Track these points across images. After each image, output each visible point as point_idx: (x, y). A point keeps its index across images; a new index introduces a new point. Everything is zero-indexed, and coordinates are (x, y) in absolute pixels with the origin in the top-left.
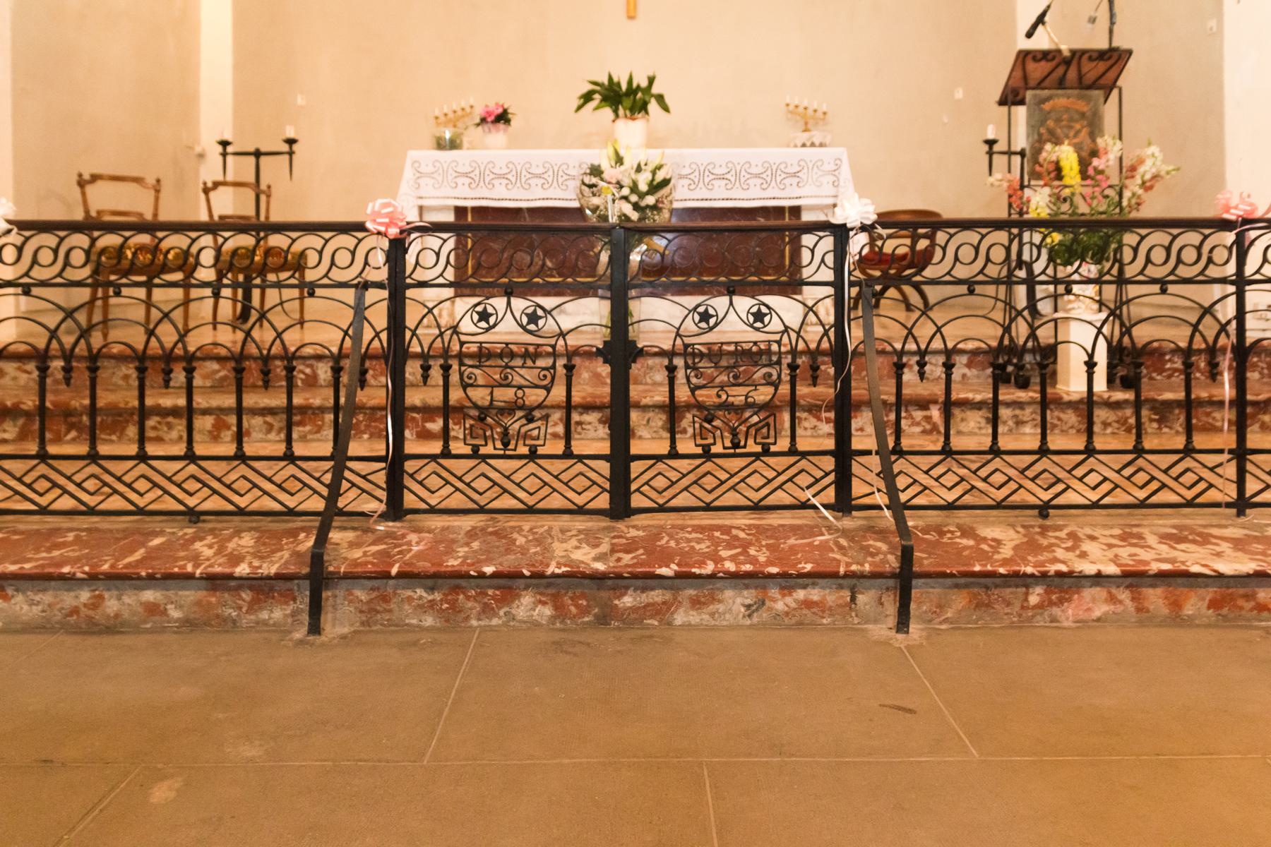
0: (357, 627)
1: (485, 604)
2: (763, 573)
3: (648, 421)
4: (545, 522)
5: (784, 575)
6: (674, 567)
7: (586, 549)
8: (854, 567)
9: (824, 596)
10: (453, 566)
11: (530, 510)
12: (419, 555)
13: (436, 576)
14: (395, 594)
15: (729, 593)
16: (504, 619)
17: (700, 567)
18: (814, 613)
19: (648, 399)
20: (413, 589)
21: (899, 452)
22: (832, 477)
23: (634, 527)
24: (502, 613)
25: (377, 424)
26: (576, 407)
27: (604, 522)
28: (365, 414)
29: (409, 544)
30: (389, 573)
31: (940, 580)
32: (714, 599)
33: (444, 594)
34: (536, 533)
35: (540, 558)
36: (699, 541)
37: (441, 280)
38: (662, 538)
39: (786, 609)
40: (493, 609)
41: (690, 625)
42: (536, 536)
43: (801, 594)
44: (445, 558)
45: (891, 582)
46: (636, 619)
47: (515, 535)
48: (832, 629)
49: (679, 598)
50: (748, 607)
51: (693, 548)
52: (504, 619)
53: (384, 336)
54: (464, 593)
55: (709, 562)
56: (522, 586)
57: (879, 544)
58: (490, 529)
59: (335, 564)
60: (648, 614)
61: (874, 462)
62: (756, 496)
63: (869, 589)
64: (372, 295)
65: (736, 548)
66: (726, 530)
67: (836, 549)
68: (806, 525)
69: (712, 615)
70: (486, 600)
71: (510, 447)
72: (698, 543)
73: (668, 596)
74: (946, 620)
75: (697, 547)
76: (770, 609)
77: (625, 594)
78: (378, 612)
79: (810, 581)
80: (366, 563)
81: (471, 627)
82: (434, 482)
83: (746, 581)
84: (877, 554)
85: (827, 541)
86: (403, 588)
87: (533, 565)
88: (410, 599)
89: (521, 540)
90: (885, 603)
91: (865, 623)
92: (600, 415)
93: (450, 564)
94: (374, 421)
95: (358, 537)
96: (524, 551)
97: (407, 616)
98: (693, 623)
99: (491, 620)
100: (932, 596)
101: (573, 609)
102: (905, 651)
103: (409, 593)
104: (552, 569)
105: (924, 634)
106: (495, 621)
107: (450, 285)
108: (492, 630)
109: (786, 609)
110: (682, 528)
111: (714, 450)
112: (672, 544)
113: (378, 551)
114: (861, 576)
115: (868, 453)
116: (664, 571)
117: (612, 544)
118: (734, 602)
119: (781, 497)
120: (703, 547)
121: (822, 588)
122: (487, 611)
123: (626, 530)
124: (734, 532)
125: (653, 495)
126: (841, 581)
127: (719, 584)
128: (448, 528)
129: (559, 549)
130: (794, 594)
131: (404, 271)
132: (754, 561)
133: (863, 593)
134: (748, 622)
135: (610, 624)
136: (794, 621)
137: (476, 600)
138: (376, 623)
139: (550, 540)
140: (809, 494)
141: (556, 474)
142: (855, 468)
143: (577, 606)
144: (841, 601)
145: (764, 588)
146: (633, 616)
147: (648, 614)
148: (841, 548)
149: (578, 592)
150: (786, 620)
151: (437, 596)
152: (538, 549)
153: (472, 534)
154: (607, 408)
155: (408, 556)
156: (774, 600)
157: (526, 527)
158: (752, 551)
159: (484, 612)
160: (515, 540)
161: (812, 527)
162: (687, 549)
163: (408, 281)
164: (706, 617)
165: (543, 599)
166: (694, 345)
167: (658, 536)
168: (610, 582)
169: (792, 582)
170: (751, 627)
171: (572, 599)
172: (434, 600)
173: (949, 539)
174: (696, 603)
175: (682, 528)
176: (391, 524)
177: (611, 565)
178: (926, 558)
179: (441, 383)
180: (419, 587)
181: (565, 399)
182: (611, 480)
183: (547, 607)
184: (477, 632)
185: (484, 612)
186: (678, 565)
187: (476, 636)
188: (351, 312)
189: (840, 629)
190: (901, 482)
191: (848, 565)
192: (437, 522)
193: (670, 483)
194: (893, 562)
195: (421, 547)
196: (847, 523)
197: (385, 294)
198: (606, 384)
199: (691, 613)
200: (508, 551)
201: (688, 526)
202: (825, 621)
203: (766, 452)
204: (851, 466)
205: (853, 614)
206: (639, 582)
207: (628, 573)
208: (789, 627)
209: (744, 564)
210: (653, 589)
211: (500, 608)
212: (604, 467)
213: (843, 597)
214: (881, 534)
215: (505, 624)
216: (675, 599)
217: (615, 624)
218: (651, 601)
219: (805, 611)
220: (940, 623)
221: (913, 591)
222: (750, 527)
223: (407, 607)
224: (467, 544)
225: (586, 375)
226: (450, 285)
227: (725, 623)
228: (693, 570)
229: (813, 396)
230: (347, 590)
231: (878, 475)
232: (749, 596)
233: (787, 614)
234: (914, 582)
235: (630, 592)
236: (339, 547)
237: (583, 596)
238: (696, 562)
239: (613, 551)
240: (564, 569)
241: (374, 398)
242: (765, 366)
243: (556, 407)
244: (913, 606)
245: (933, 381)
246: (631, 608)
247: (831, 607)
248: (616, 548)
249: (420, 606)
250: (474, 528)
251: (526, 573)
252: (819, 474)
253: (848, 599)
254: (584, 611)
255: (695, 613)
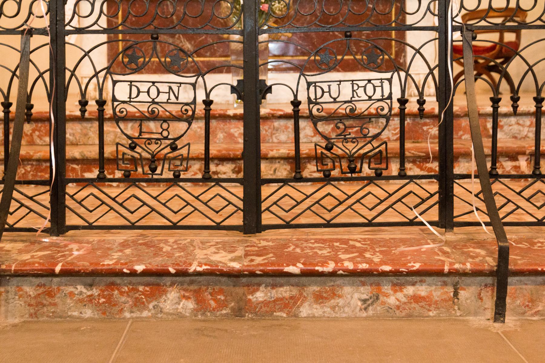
0: (27, 318)
1: (136, 298)
2: (377, 271)
3: (275, 171)
4: (187, 237)
5: (396, 273)
6: (300, 266)
7: (224, 253)
8: (457, 266)
9: (431, 291)
10: (109, 265)
11: (175, 226)
12: (79, 258)
13: (94, 274)
14: (59, 290)
15: (347, 289)
16: (153, 312)
17: (322, 266)
18: (422, 307)
19: (275, 152)
20: (75, 286)
21: (496, 177)
22: (436, 198)
23: (264, 240)
24: (151, 306)
25: (43, 174)
26: (213, 159)
27: (238, 236)
28: (32, 165)
29: (71, 250)
30: (54, 270)
31: (533, 278)
32: (335, 294)
33: (101, 290)
34: (180, 244)
35: (184, 259)
36: (321, 249)
37: (95, 28)
38: (289, 247)
39: (398, 303)
40: (143, 303)
41: (314, 317)
42: (181, 246)
43: (410, 290)
44: (102, 260)
45: (489, 280)
46: (267, 312)
47: (162, 245)
48: (437, 319)
49: (305, 294)
50: (365, 301)
51: (316, 253)
52: (153, 312)
53: (47, 76)
54: (118, 289)
55: (330, 262)
56: (168, 283)
57: (478, 250)
58: (140, 242)
59: (7, 263)
60: (277, 307)
61: (475, 185)
62: (370, 215)
63: (469, 285)
64: (36, 40)
65: (353, 253)
66: (345, 242)
67: (440, 254)
68: (414, 239)
69: (333, 308)
70: (137, 295)
71: (156, 173)
72: (320, 250)
73: (295, 291)
74: (537, 313)
75: (320, 252)
76: (383, 303)
77: (258, 290)
78: (44, 305)
79: (418, 279)
80: (34, 263)
81: (124, 318)
82: (90, 203)
83: (363, 279)
84: (477, 257)
85: (432, 249)
86: (66, 285)
87: (178, 264)
88: (71, 294)
89: (166, 248)
90: (484, 298)
91: (466, 316)
92: (234, 166)
93: (106, 263)
94: (40, 172)
95: (26, 246)
96: (169, 255)
97: (70, 308)
98: (316, 315)
99: (142, 312)
100: (525, 292)
101: (212, 303)
102: (502, 335)
103: (71, 289)
104: (194, 267)
105: (518, 323)
106: (145, 314)
107: (104, 31)
108: (143, 321)
109: (398, 303)
110: (307, 241)
111: (335, 173)
112: (298, 250)
113: (44, 255)
114: (464, 274)
115: (468, 176)
116: (291, 269)
117: (245, 251)
118: (352, 297)
119: (391, 217)
120: (325, 252)
121: (429, 285)
122: (138, 304)
123: (257, 242)
124: (351, 243)
125: (282, 213)
126: (445, 279)
127: (339, 281)
128: (104, 240)
129: (200, 254)
130: (405, 290)
131: (64, 20)
132: (369, 261)
133: (464, 290)
134: (364, 314)
135: (244, 316)
136: (404, 314)
137: (128, 296)
138: (42, 315)
139: (192, 248)
140: (416, 212)
141: (196, 195)
142: (457, 190)
143: (215, 300)
144: (444, 297)
145: (378, 285)
146: (264, 309)
147: (277, 307)
148: (445, 253)
149: (217, 288)
150: (397, 312)
151: (95, 292)
152: (182, 253)
153: (124, 245)
154: (239, 159)
155: (70, 258)
156: (387, 296)
157: (171, 240)
158: (367, 255)
159: (135, 305)
160: (162, 248)
161: (419, 240)
162: (311, 254)
163: (68, 28)
164: (328, 310)
165: (187, 294)
166: (315, 83)
167: (286, 246)
168: (244, 280)
169: (402, 279)
170: (366, 318)
171: (211, 294)
172: (92, 295)
173: (539, 247)
174: (319, 298)
175: (307, 241)
176: (55, 238)
177: (246, 264)
178: (520, 260)
179: (97, 142)
180: (79, 284)
181: (203, 152)
182: (244, 200)
183: (190, 301)
184: (130, 322)
185: (135, 305)
186: (303, 264)
187: (128, 325)
188: (19, 55)
189: (444, 320)
190: (499, 201)
191: (451, 264)
192: (94, 237)
193: (295, 203)
194: (491, 262)
195: (81, 252)
196: (450, 236)
197: (47, 39)
198: (239, 143)
199: (315, 306)
200: (156, 255)
201: (311, 239)
202: (431, 314)
203: (379, 175)
204: (453, 187)
205: (456, 307)
206: (269, 280)
207: (260, 271)
208: (400, 319)
209: (360, 263)
210: (281, 286)
211: (149, 303)
212: (239, 190)
213: (447, 292)
214: (481, 244)
215: (154, 316)
216: (301, 294)
217: (249, 316)
218: (280, 296)
219: (413, 305)
220: (532, 315)
221: (509, 288)
222: (365, 240)
223: (69, 301)
224: (121, 251)
225: (221, 135)
226: (104, 31)
227: (344, 315)
228: (317, 268)
229: (417, 149)
230: (18, 286)
231: (476, 196)
232: (365, 292)
233: (398, 307)
234: (510, 280)
235: (262, 288)
236: (11, 253)
237: (221, 292)
238: (319, 262)
239: (246, 255)
240: (204, 267)
241: (39, 152)
242: (379, 100)
243: (197, 159)
244: (508, 300)
245: (521, 139)
246: (262, 302)
247: (437, 301)
248: (249, 253)
249: (81, 301)
250: (126, 241)
251: (172, 271)
252: (425, 195)
253: (452, 294)
254: (222, 305)
255: (318, 306)
